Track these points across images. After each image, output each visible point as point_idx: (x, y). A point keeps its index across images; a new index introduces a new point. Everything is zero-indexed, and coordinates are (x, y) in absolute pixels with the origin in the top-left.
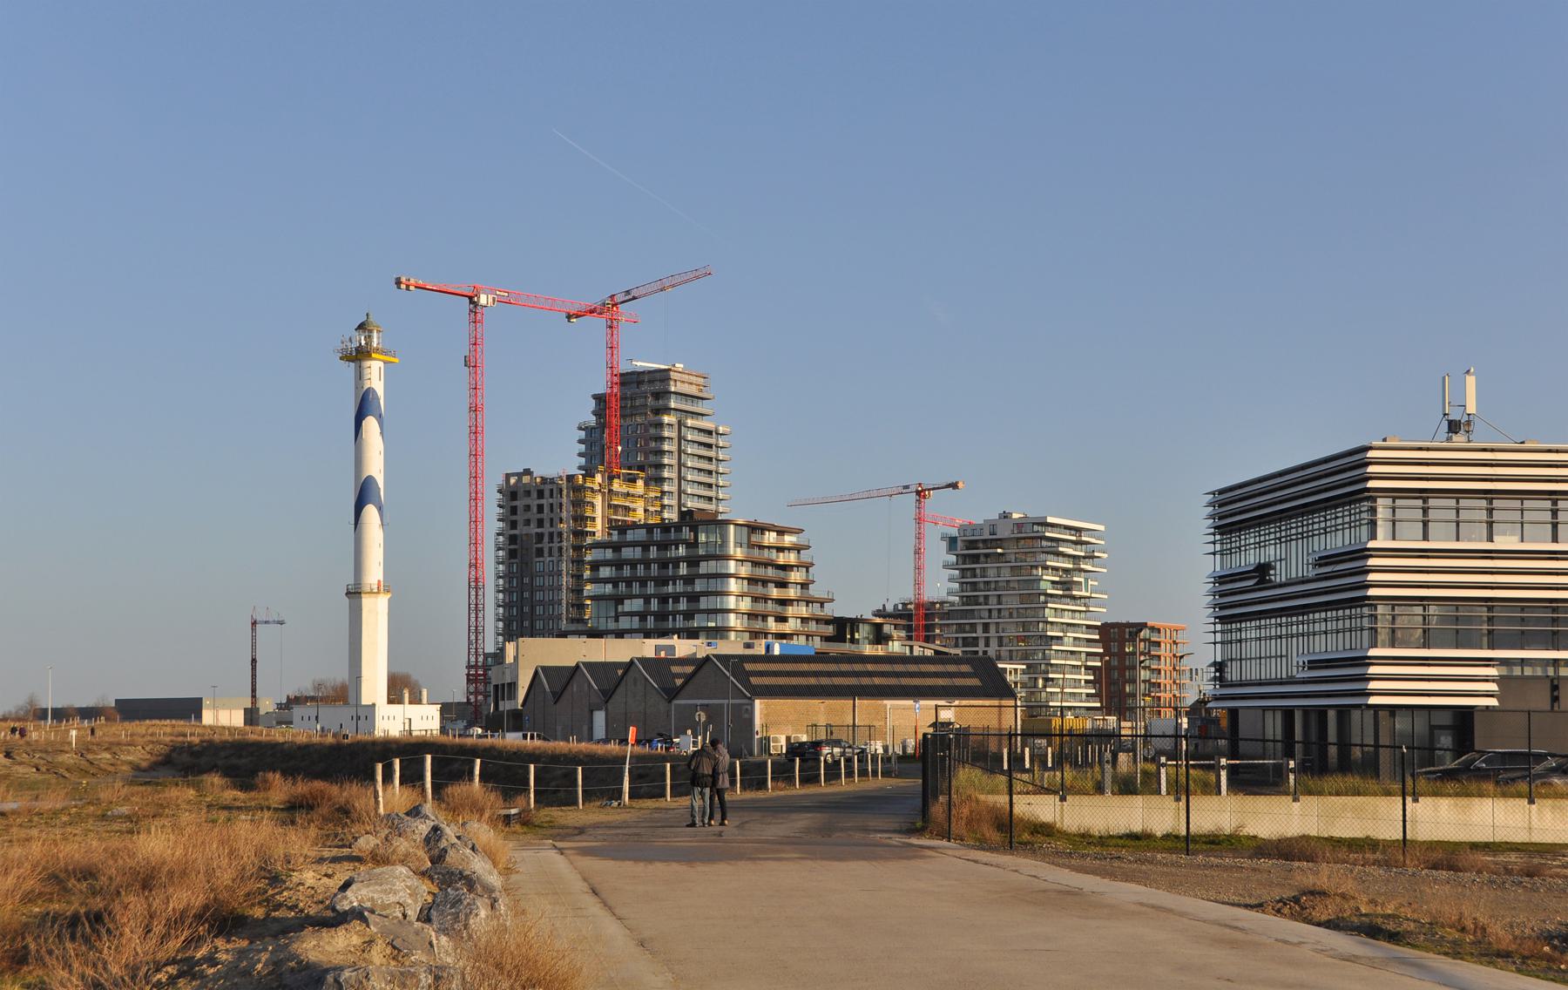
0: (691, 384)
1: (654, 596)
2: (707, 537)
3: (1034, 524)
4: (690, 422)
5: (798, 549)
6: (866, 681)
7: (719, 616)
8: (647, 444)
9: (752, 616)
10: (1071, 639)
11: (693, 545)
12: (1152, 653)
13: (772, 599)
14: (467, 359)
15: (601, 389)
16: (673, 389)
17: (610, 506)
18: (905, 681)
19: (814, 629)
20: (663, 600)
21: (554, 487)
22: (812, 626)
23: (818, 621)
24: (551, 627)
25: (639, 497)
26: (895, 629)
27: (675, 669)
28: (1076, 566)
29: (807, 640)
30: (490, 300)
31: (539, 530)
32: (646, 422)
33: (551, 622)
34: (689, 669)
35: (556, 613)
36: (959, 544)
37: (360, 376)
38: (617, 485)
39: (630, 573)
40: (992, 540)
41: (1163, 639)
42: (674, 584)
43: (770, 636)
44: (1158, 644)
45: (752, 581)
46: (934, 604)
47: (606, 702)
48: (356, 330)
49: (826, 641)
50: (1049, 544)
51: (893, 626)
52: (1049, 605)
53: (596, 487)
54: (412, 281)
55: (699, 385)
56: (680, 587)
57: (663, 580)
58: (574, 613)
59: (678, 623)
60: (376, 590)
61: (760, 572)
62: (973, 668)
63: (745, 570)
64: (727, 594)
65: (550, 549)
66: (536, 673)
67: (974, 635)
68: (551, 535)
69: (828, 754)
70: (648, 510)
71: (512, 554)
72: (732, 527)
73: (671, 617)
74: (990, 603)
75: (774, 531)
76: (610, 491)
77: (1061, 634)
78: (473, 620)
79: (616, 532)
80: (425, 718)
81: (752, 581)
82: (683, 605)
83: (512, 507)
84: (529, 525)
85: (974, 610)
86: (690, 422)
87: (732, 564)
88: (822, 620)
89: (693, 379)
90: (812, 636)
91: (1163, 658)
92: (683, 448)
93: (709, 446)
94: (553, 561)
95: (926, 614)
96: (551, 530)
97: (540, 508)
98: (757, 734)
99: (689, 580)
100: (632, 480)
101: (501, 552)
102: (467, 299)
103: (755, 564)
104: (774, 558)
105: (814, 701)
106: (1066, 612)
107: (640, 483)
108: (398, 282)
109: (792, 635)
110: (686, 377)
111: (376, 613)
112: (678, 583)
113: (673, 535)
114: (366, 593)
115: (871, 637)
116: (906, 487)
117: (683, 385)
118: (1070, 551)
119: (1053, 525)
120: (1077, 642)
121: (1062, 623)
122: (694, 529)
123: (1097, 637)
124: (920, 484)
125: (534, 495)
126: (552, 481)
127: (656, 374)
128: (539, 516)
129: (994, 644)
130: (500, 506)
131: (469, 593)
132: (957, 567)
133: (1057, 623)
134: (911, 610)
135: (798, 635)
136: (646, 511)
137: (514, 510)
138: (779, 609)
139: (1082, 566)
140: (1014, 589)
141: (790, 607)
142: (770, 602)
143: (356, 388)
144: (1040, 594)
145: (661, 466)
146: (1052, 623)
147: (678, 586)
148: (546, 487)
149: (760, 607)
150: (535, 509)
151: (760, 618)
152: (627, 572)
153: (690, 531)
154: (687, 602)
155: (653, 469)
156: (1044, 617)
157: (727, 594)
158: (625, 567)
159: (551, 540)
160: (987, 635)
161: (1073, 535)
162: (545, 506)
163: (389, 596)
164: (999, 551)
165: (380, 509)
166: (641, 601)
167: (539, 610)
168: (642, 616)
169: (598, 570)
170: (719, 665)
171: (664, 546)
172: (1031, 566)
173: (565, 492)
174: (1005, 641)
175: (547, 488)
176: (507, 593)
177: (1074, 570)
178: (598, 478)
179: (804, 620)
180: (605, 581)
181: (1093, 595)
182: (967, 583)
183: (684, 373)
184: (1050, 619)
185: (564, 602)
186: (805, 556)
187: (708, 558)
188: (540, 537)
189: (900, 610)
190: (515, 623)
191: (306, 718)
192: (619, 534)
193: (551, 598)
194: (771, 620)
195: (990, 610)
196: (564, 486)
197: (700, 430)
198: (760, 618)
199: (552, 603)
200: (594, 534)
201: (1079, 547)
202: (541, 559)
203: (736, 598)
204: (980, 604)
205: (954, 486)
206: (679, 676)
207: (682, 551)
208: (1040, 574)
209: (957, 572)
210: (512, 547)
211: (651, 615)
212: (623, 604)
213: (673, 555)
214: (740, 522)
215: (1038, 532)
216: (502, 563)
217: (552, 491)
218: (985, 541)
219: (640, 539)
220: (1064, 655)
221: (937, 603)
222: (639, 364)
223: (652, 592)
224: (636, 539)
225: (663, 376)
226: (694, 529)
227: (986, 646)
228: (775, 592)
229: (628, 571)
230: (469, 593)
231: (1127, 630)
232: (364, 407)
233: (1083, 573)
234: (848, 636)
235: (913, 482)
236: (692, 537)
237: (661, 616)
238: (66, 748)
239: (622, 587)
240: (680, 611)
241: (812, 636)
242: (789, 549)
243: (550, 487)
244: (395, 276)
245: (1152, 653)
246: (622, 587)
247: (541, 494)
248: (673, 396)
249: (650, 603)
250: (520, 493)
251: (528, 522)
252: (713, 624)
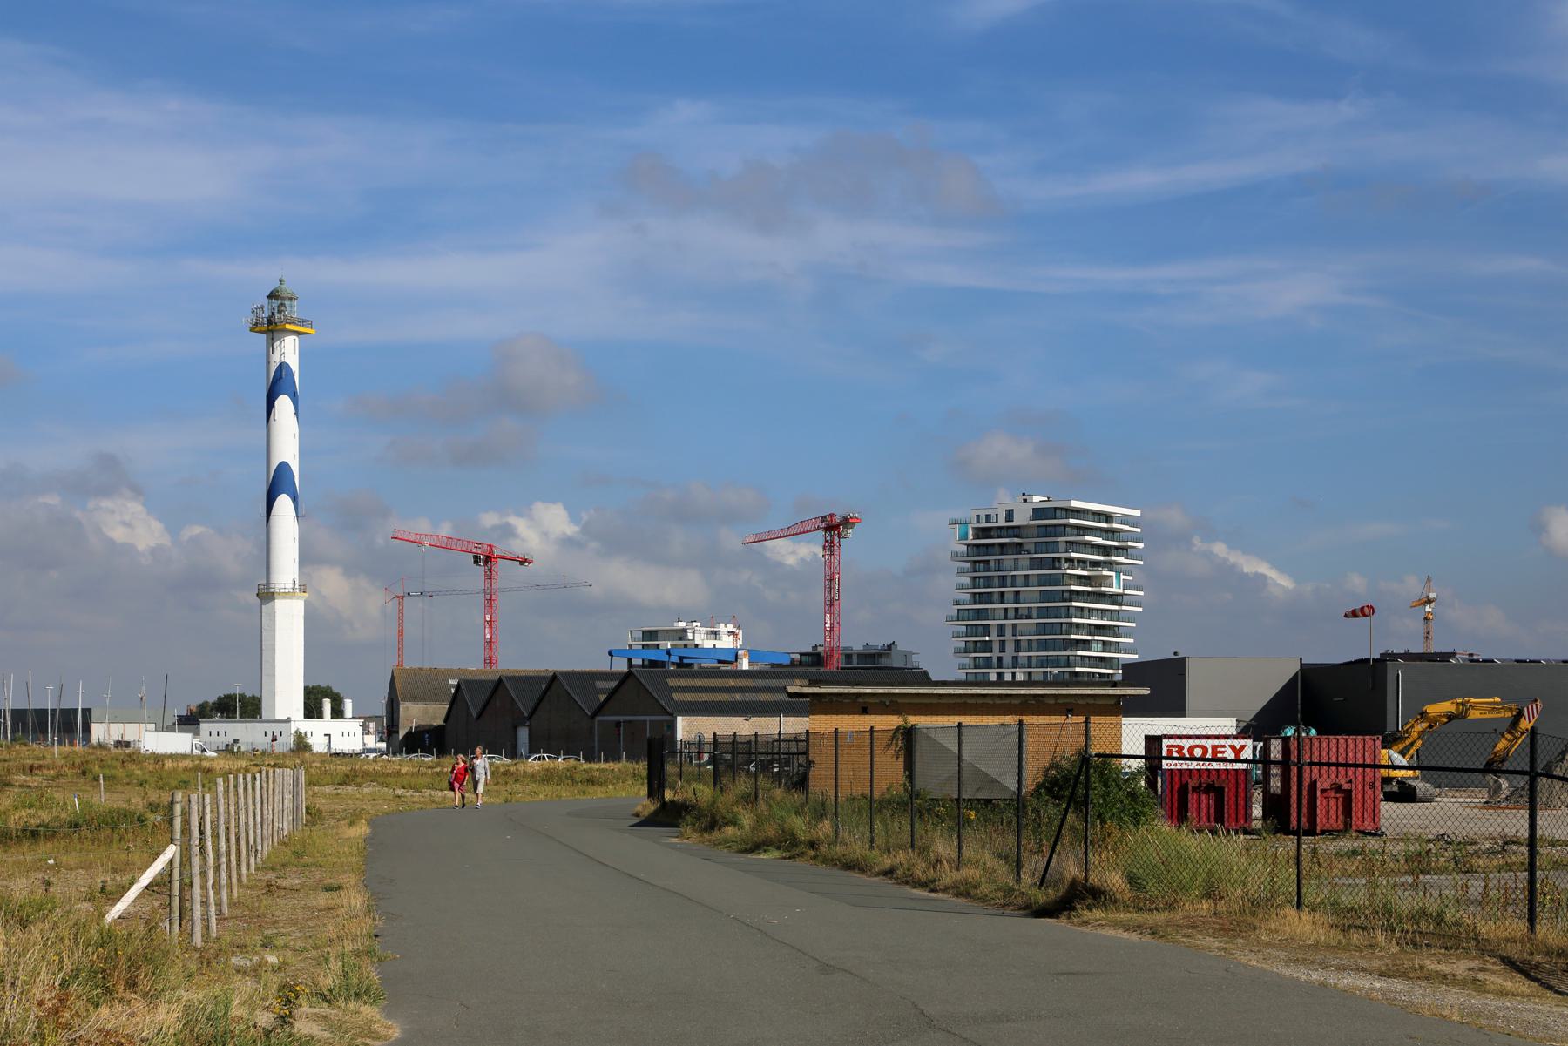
27: (600, 685)
40: (1008, 527)
80: (346, 734)
85: (987, 609)
132: (969, 558)
160: (1001, 638)
165: (295, 499)
195: (1006, 610)
206: (602, 691)
209: (968, 565)
218: (1000, 528)
227: (1016, 657)
232: (278, 383)
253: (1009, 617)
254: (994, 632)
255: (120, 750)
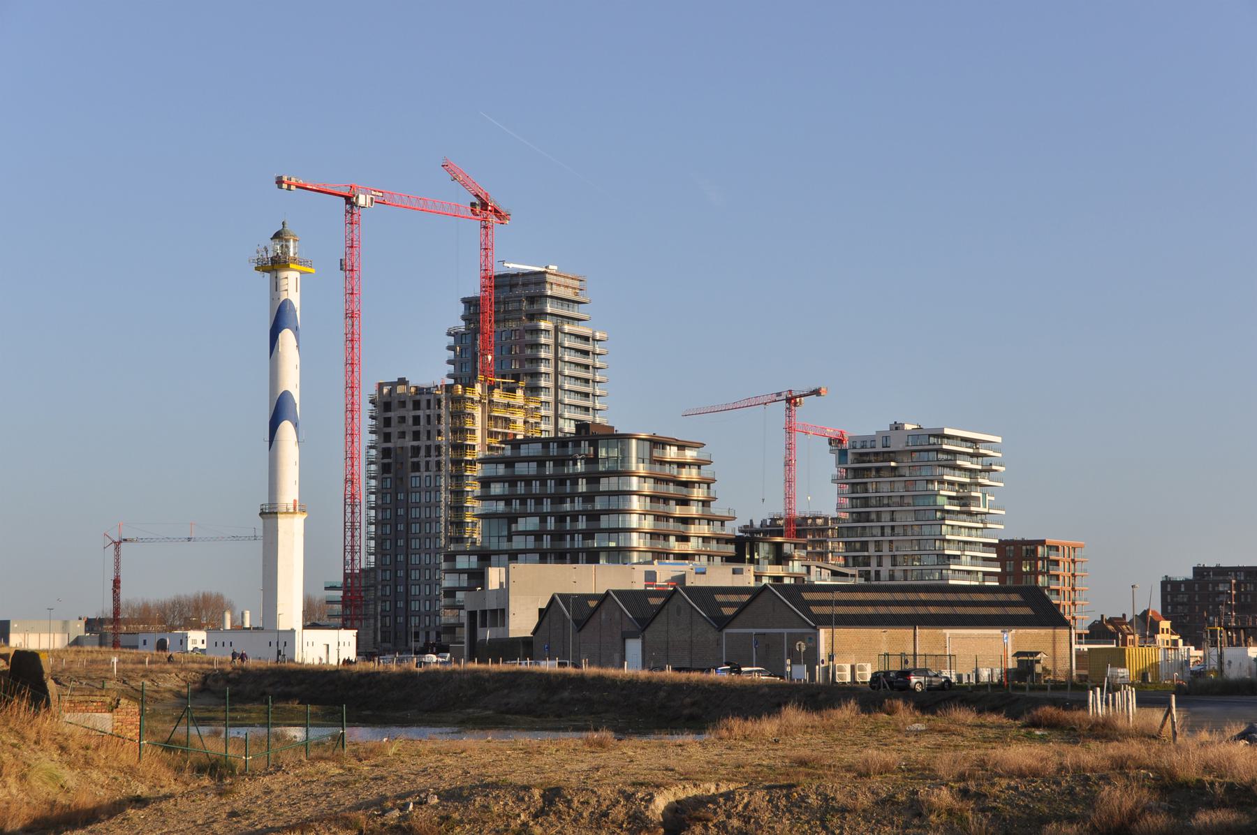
0: (567, 287)
1: (551, 514)
2: (607, 452)
3: (930, 436)
4: (567, 328)
5: (698, 464)
6: (922, 610)
7: (622, 536)
8: (522, 351)
9: (654, 535)
10: (969, 558)
11: (593, 460)
12: (1051, 572)
13: (674, 518)
14: (343, 263)
15: (474, 290)
16: (549, 293)
17: (490, 418)
18: (960, 610)
19: (715, 549)
20: (561, 518)
21: (432, 398)
22: (713, 546)
23: (719, 540)
24: (428, 547)
25: (519, 407)
26: (795, 548)
28: (973, 480)
29: (709, 560)
30: (369, 200)
31: (415, 443)
32: (522, 328)
33: (428, 540)
34: (746, 598)
35: (433, 531)
36: (850, 457)
37: (276, 287)
38: (498, 396)
39: (525, 490)
40: (884, 452)
41: (1060, 558)
42: (572, 502)
43: (672, 556)
44: (1057, 563)
45: (654, 498)
46: (805, 519)
47: (644, 630)
48: (272, 239)
49: (726, 561)
50: (945, 457)
51: (793, 546)
52: (947, 522)
53: (477, 398)
54: (293, 180)
55: (575, 288)
56: (578, 505)
57: (561, 498)
58: (452, 531)
59: (576, 543)
60: (292, 510)
61: (663, 489)
62: (1023, 596)
63: (648, 487)
64: (629, 512)
65: (427, 463)
66: (553, 599)
67: (866, 554)
68: (428, 448)
69: (916, 683)
70: (528, 422)
71: (385, 468)
72: (634, 442)
73: (568, 537)
74: (883, 520)
75: (674, 445)
76: (491, 402)
77: (958, 553)
78: (349, 538)
79: (509, 447)
81: (654, 498)
82: (582, 524)
83: (385, 418)
84: (405, 438)
86: (567, 328)
87: (635, 480)
88: (723, 539)
89: (570, 282)
90: (713, 556)
91: (1061, 578)
92: (560, 355)
93: (586, 353)
94: (430, 477)
95: (797, 530)
96: (428, 443)
97: (416, 420)
98: (823, 663)
99: (589, 497)
100: (511, 390)
101: (372, 466)
102: (343, 199)
103: (658, 480)
104: (675, 474)
105: (876, 630)
106: (963, 530)
107: (520, 393)
108: (280, 182)
109: (693, 555)
110: (561, 280)
111: (292, 532)
112: (576, 501)
113: (570, 450)
114: (282, 513)
115: (771, 557)
116: (779, 394)
117: (558, 288)
118: (968, 465)
119: (949, 437)
120: (974, 561)
121: (959, 541)
122: (594, 443)
123: (995, 556)
124: (790, 391)
125: (410, 405)
126: (429, 391)
127: (530, 277)
128: (416, 428)
129: (887, 563)
130: (372, 418)
131: (345, 511)
133: (954, 540)
134: (780, 526)
135: (699, 555)
136: (525, 422)
137: (387, 422)
138: (681, 527)
139: (980, 480)
140: (909, 505)
141: (693, 526)
142: (671, 520)
143: (272, 299)
144: (936, 510)
145: (537, 375)
146: (949, 541)
147: (576, 504)
148: (422, 397)
149: (663, 526)
150: (410, 421)
151: (661, 537)
152: (521, 488)
153: (590, 446)
154: (587, 520)
155: (529, 378)
156: (941, 535)
157: (629, 512)
158: (519, 483)
159: (428, 454)
161: (970, 448)
162: (421, 417)
163: (305, 516)
164: (893, 464)
165: (296, 426)
166: (536, 520)
167: (415, 528)
168: (538, 535)
169: (490, 487)
170: (779, 595)
171: (560, 462)
172: (927, 480)
173: (443, 403)
174: (899, 560)
175: (424, 398)
176: (380, 510)
177: (970, 484)
178: (478, 388)
179: (706, 539)
180: (497, 498)
181: (991, 511)
182: (857, 498)
183: (560, 276)
184: (948, 537)
185: (443, 519)
186: (706, 471)
187: (609, 474)
188: (416, 451)
189: (768, 526)
190: (388, 542)
191: (220, 644)
192: (512, 449)
193: (428, 516)
194: (672, 539)
195: (883, 528)
196: (443, 397)
197: (577, 336)
198: (661, 537)
199: (429, 520)
200: (473, 447)
201: (975, 459)
202: (417, 474)
203: (638, 514)
204: (872, 521)
205: (817, 392)
207: (580, 467)
208: (936, 489)
210: (386, 461)
211: (547, 535)
212: (517, 522)
213: (571, 471)
214: (643, 436)
215: (934, 444)
216: (374, 478)
217: (429, 401)
218: (877, 454)
219: (536, 454)
220: (961, 575)
221: (809, 518)
222: (511, 266)
223: (549, 510)
224: (530, 455)
225: (538, 279)
226: (594, 443)
227: (879, 571)
228: (678, 511)
229: (523, 488)
230: (345, 511)
231: (1024, 548)
232: (280, 319)
233: (979, 488)
234: (748, 556)
235: (784, 388)
236: (592, 452)
237: (558, 536)
238: (109, 675)
239: (516, 504)
240: (579, 530)
241: (713, 556)
242: (690, 464)
243: (428, 397)
244: (276, 175)
245: (1051, 572)
246: (516, 504)
247: (417, 405)
248: (549, 300)
249: (546, 522)
250: (395, 403)
251: (402, 435)
252: (613, 544)
253: (886, 534)
254: (872, 548)
255: (863, 685)
